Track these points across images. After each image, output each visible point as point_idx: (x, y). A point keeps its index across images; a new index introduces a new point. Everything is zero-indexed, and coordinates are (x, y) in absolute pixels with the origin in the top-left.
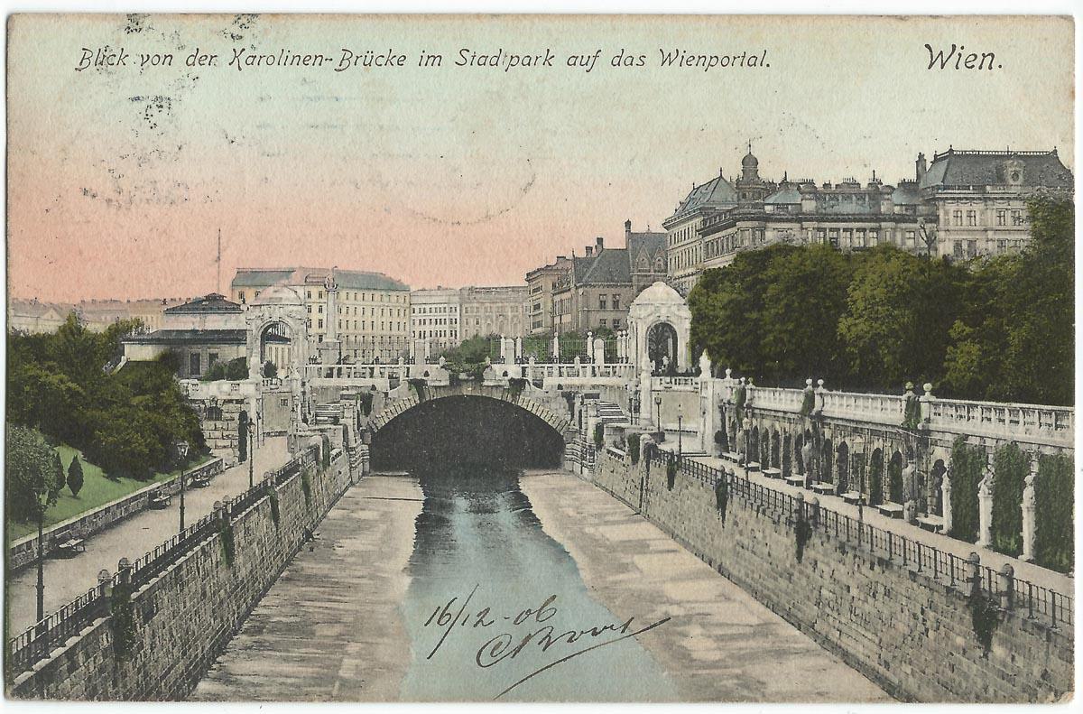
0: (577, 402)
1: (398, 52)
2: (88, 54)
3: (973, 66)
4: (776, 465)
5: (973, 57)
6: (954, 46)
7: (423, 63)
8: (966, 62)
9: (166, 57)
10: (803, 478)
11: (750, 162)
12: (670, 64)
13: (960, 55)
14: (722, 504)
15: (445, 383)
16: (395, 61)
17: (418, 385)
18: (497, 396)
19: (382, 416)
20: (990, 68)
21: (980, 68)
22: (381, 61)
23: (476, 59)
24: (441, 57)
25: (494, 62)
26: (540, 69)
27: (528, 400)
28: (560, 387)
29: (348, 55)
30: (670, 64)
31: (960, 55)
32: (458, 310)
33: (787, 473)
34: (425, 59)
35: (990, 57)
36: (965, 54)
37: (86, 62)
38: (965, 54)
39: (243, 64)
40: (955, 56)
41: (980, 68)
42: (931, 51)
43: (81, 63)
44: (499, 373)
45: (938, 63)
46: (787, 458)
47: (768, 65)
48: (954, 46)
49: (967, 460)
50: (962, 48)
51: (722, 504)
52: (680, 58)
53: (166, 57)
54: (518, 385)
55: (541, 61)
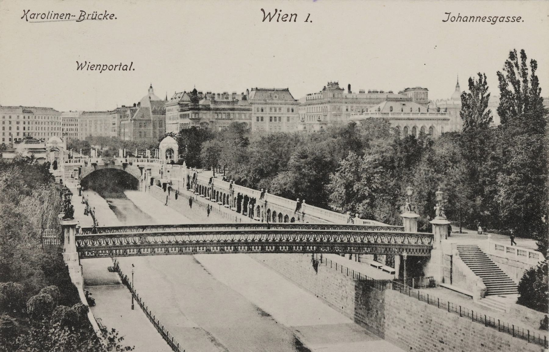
0: (144, 171)
1: (110, 12)
2: (83, 13)
3: (286, 20)
4: (203, 194)
5: (286, 16)
6: (276, 10)
7: (294, 17)
8: (282, 18)
9: (95, 18)
10: (209, 198)
13: (279, 14)
14: (191, 204)
15: (103, 164)
16: (108, 17)
17: (94, 165)
18: (118, 168)
19: (84, 175)
21: (290, 21)
22: (101, 17)
24: (296, 15)
27: (129, 170)
28: (138, 166)
29: (83, 13)
31: (279, 14)
33: (205, 196)
34: (53, 15)
35: (295, 16)
36: (282, 14)
37: (82, 18)
38: (282, 14)
40: (277, 15)
41: (290, 21)
43: (79, 19)
44: (120, 161)
46: (205, 193)
47: (311, 22)
49: (240, 197)
50: (281, 11)
51: (191, 204)
52: (277, 15)
54: (125, 165)
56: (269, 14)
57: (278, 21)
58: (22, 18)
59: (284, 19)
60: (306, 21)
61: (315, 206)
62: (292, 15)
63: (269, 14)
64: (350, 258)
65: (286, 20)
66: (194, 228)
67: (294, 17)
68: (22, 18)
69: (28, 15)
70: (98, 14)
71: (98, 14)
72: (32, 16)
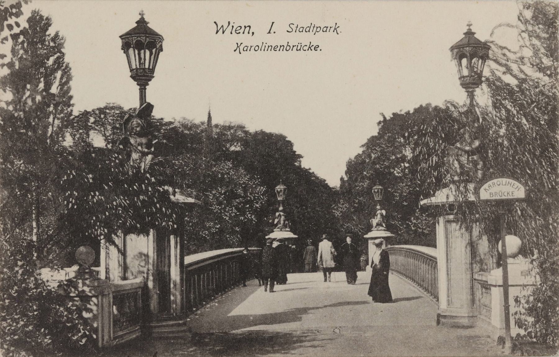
1: (314, 44)
3: (239, 33)
6: (229, 23)
9: (300, 50)
11: (469, 34)
12: (223, 32)
13: (233, 27)
16: (313, 48)
20: (249, 33)
21: (243, 33)
23: (298, 29)
24: (250, 27)
25: (307, 30)
26: (331, 34)
30: (223, 32)
31: (233, 27)
32: (512, 302)
35: (248, 28)
39: (241, 51)
40: (230, 27)
41: (243, 33)
42: (217, 25)
45: (221, 31)
48: (229, 23)
52: (230, 27)
53: (300, 50)
55: (332, 29)
56: (222, 26)
57: (231, 33)
58: (235, 51)
59: (238, 32)
60: (269, 33)
61: (338, 271)
62: (245, 27)
63: (222, 26)
64: (266, 290)
65: (239, 33)
66: (290, 288)
67: (248, 29)
68: (235, 51)
69: (241, 48)
70: (303, 45)
71: (303, 45)
72: (245, 49)
